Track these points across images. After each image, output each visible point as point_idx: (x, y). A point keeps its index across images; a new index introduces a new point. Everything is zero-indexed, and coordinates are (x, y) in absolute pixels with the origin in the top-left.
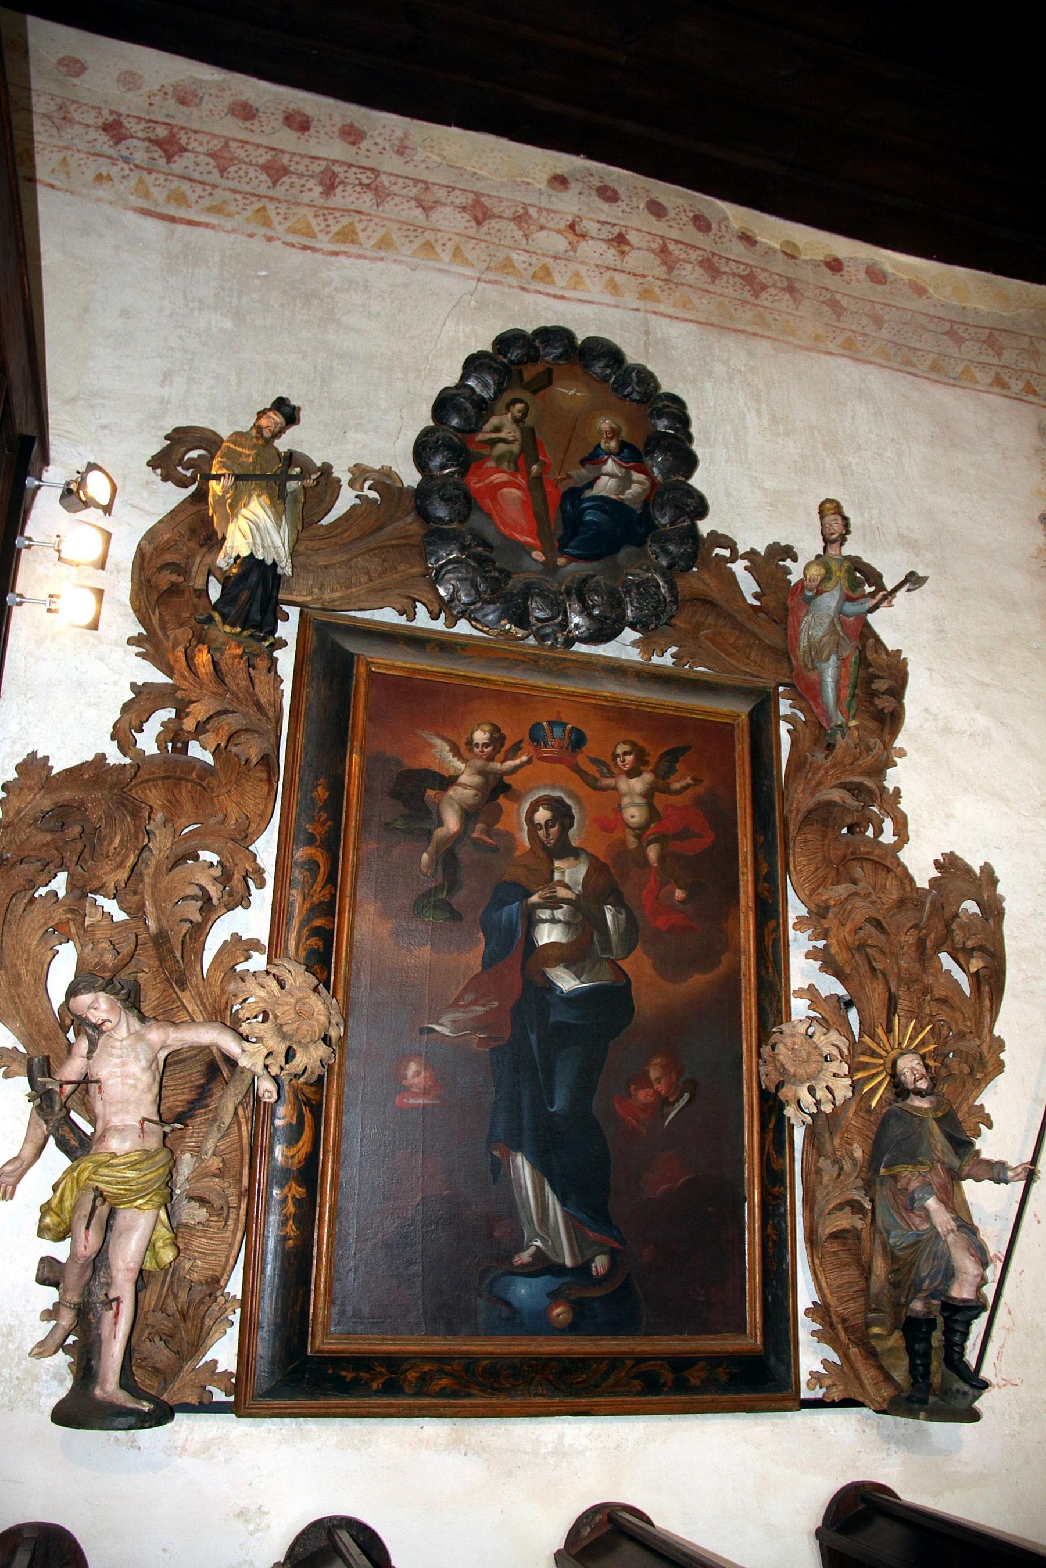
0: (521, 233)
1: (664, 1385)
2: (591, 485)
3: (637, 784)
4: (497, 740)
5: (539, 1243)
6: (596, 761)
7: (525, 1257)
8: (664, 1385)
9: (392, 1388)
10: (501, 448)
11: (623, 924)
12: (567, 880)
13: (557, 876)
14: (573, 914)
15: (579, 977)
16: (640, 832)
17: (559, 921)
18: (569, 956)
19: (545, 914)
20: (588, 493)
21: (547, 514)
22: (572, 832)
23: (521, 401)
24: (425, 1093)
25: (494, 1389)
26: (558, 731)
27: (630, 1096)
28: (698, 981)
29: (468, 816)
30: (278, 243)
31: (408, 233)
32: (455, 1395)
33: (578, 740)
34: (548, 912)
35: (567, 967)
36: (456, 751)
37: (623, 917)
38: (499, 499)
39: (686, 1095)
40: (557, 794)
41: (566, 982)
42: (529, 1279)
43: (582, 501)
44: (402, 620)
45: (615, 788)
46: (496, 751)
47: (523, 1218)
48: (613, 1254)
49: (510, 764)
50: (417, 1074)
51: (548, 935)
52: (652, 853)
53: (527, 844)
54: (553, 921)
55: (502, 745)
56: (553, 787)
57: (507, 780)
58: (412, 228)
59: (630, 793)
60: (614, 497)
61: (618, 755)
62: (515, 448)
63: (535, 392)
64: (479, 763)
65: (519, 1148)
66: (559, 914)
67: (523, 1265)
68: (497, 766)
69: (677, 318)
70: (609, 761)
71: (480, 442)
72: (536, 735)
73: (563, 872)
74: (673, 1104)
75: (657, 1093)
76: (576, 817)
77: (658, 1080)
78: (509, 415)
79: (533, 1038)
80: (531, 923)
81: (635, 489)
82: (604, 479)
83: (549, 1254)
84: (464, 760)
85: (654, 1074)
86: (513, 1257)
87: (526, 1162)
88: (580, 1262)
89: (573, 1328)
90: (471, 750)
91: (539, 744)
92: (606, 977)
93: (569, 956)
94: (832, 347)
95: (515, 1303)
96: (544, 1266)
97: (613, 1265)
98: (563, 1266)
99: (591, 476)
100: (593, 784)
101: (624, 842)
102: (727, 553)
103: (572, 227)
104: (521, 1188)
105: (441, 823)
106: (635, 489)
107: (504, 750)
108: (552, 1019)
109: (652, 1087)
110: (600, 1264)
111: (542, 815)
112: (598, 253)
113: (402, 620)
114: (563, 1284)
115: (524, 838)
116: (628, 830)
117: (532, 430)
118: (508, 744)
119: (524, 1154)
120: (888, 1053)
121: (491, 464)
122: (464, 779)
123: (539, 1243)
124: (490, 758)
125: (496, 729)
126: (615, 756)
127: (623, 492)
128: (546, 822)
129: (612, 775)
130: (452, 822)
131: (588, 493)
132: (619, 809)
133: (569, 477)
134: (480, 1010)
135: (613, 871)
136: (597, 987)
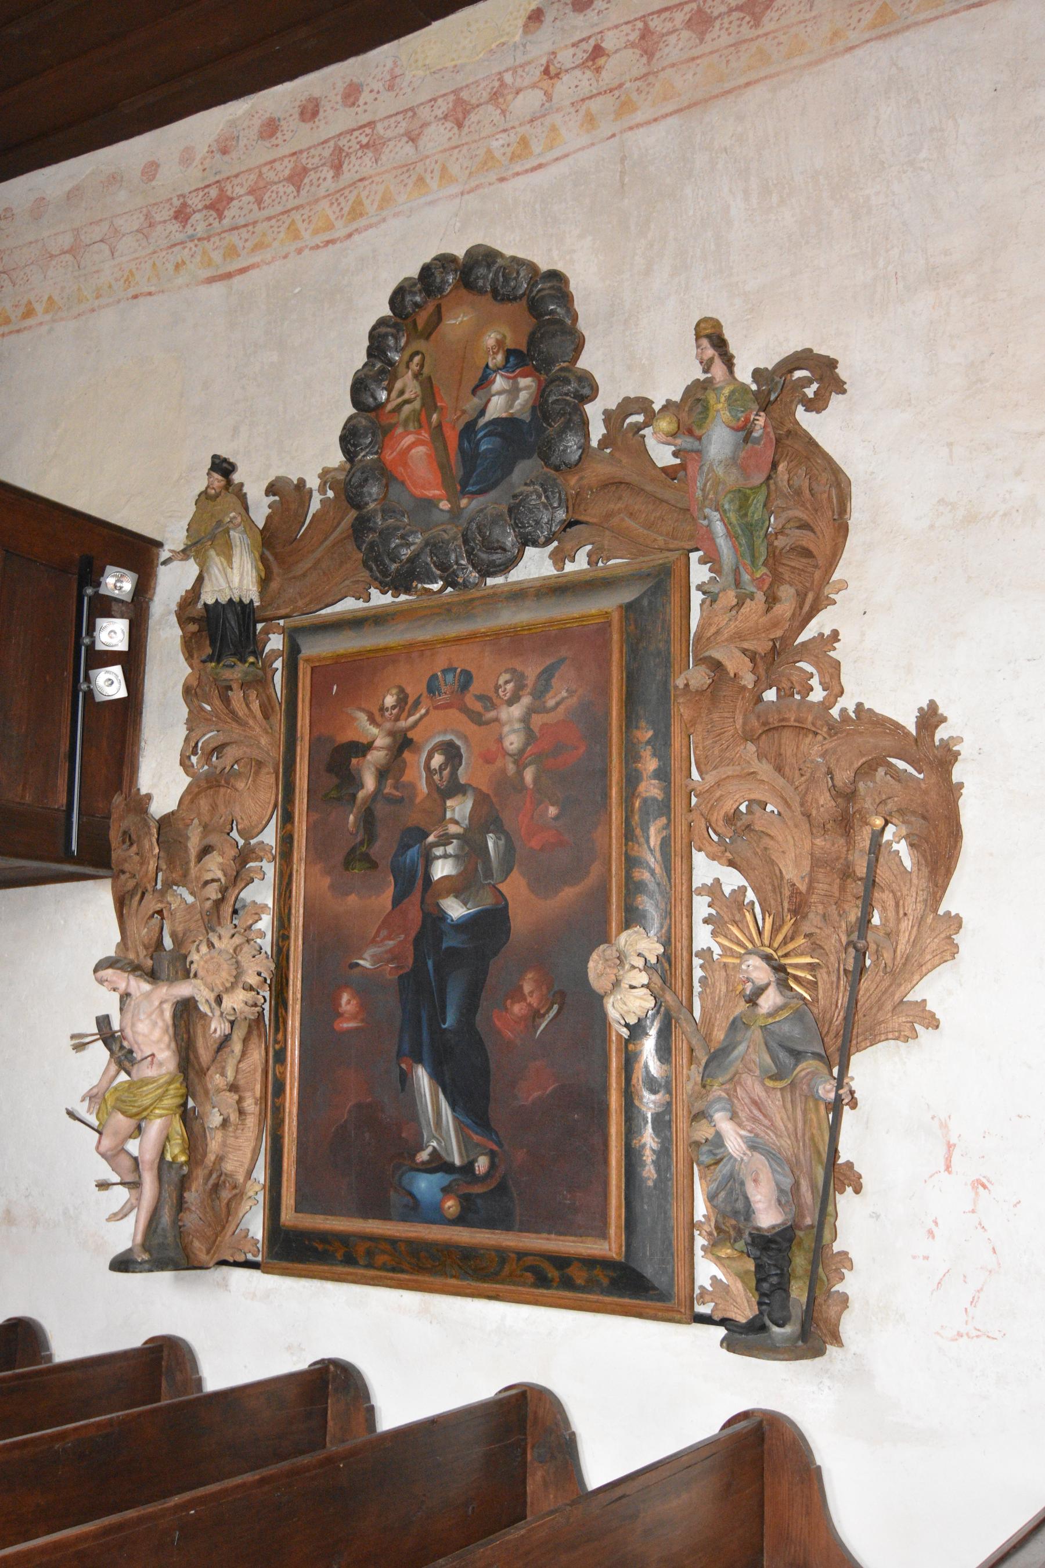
0: (499, 111)
1: (552, 1281)
2: (482, 412)
3: (516, 711)
4: (402, 700)
5: (435, 1144)
6: (480, 698)
7: (424, 1156)
8: (552, 1281)
9: (350, 1260)
10: (407, 408)
11: (502, 849)
12: (457, 817)
13: (449, 815)
14: (461, 848)
15: (465, 904)
16: (519, 759)
17: (450, 856)
18: (458, 887)
19: (439, 851)
20: (482, 422)
21: (448, 460)
22: (461, 771)
23: (417, 353)
24: (354, 1017)
25: (420, 1269)
26: (450, 677)
27: (506, 1009)
28: (569, 893)
29: (382, 775)
30: (306, 252)
31: (402, 178)
32: (393, 1270)
33: (466, 679)
34: (442, 849)
35: (456, 897)
36: (372, 720)
37: (502, 842)
38: (409, 461)
39: (556, 1007)
40: (448, 737)
41: (455, 910)
42: (428, 1175)
43: (476, 433)
44: (360, 604)
45: (497, 720)
46: (402, 710)
47: (423, 1122)
48: (492, 1155)
49: (412, 719)
50: (348, 1002)
51: (442, 869)
52: (529, 775)
53: (425, 790)
54: (446, 856)
55: (406, 703)
56: (445, 732)
57: (410, 735)
58: (405, 169)
59: (510, 721)
60: (504, 415)
61: (500, 686)
62: (417, 404)
63: (427, 338)
64: (388, 725)
65: (419, 1060)
66: (450, 849)
67: (423, 1163)
68: (403, 724)
69: (655, 120)
70: (492, 694)
71: (390, 412)
72: (432, 688)
73: (454, 810)
74: (543, 1016)
75: (530, 1005)
76: (464, 756)
77: (531, 992)
78: (410, 373)
79: (430, 963)
80: (429, 861)
81: (523, 396)
82: (494, 399)
83: (443, 1154)
84: (377, 725)
85: (527, 988)
86: (415, 1155)
87: (425, 1073)
88: (466, 1160)
89: (460, 1220)
90: (382, 716)
91: (434, 695)
92: (487, 901)
93: (458, 887)
94: (853, 37)
95: (415, 1191)
96: (439, 1164)
97: (493, 1165)
98: (453, 1164)
99: (484, 400)
100: (477, 719)
101: (503, 771)
102: (640, 418)
103: (546, 72)
104: (422, 1096)
105: (362, 786)
106: (523, 396)
107: (407, 708)
108: (444, 946)
109: (525, 1000)
110: (482, 1164)
111: (437, 760)
112: (573, 87)
113: (360, 604)
114: (455, 1180)
115: (423, 787)
116: (507, 757)
117: (430, 378)
118: (410, 701)
119: (424, 1066)
120: (763, 945)
121: (400, 430)
122: (378, 743)
123: (435, 1144)
124: (397, 719)
125: (401, 690)
126: (497, 687)
127: (511, 407)
128: (440, 766)
129: (494, 707)
130: (370, 783)
131: (482, 422)
132: (500, 740)
133: (464, 412)
134: (391, 943)
135: (494, 800)
136: (482, 911)
